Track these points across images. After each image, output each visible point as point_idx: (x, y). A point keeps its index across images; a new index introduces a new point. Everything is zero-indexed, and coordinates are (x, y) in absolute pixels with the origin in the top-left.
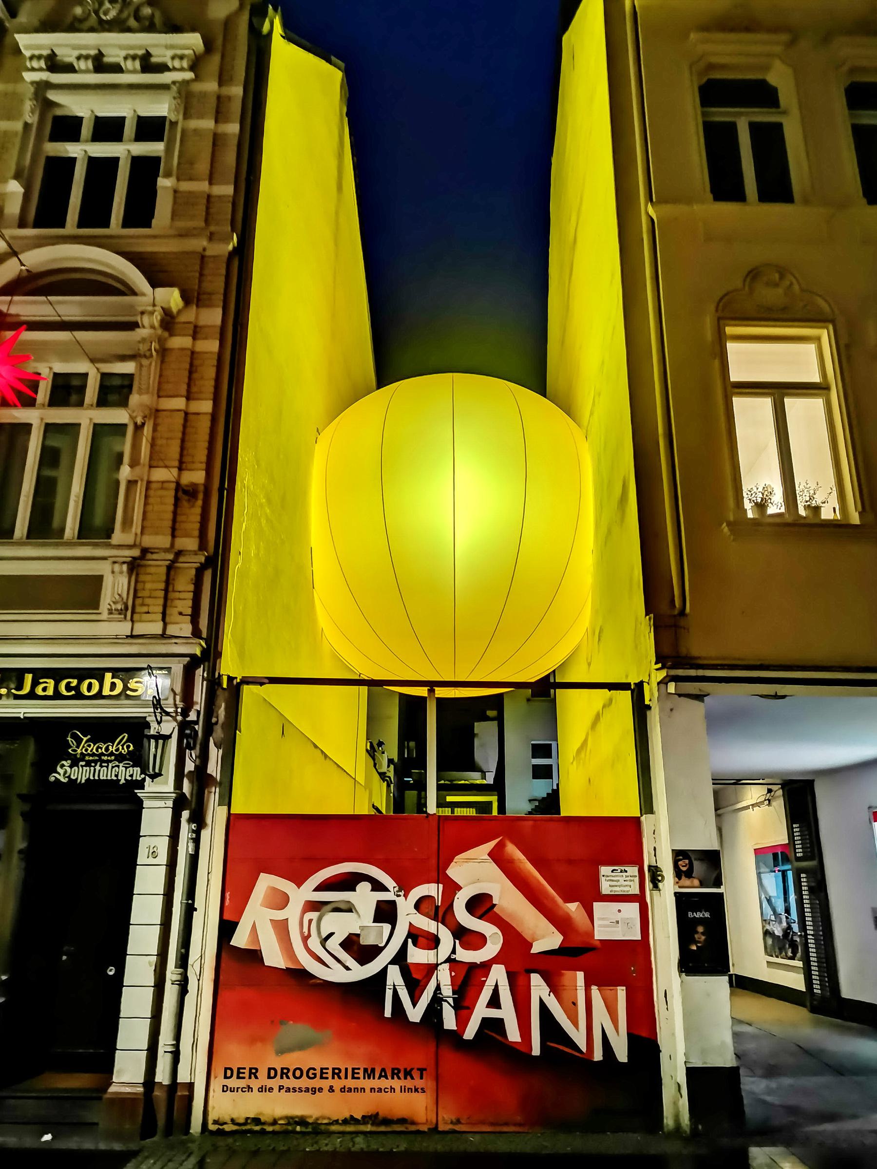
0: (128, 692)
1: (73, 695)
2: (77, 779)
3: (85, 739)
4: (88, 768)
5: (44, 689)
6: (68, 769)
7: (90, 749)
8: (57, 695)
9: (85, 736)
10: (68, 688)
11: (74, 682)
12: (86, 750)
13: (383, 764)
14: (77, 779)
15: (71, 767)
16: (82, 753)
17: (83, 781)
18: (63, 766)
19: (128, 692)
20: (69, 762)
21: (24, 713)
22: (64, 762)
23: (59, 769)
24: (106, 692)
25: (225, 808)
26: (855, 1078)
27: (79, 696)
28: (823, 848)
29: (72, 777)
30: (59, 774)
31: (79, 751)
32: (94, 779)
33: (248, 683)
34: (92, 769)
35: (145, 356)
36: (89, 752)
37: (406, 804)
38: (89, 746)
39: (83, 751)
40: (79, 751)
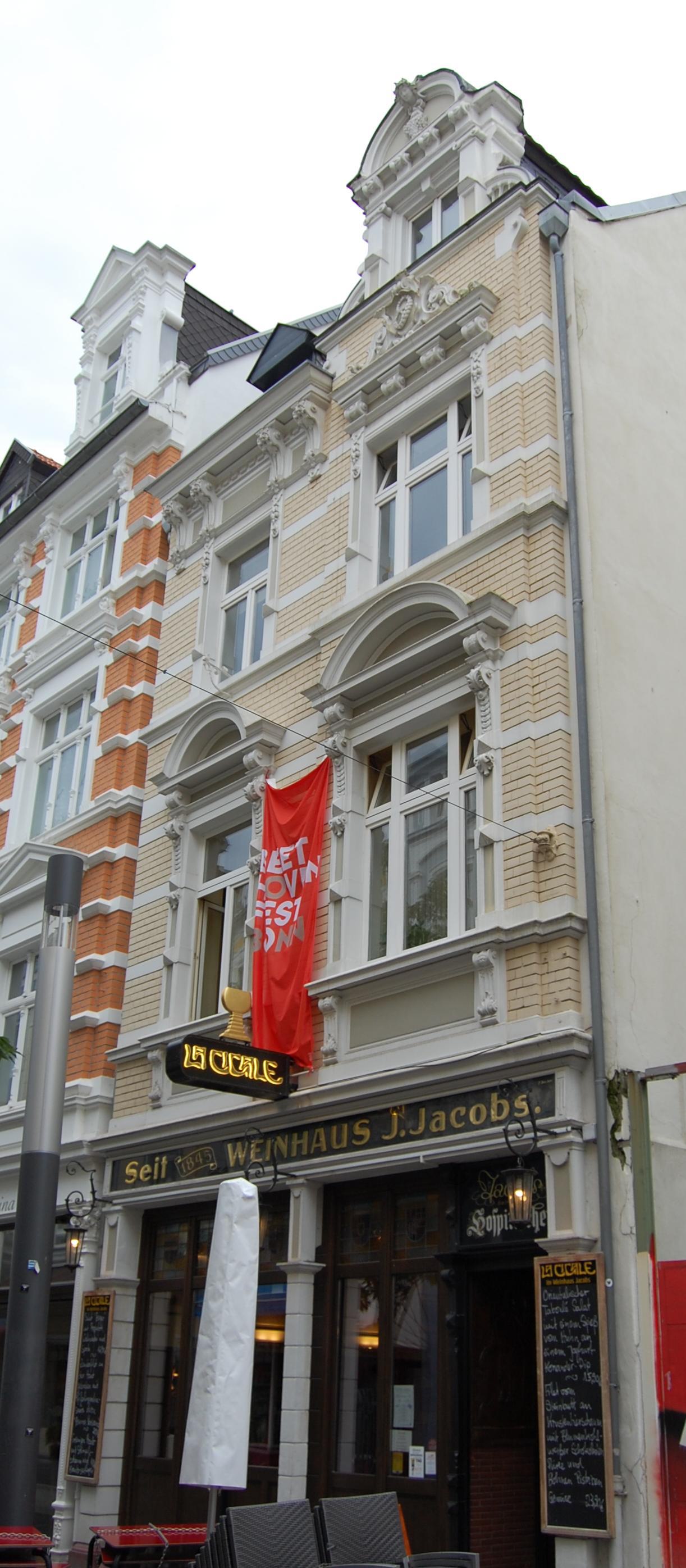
0: (516, 1114)
1: (633, 1152)
2: (492, 1231)
3: (494, 1180)
4: (501, 1216)
5: (438, 1124)
6: (483, 1219)
7: (500, 1192)
8: (451, 1130)
9: (494, 1176)
10: (459, 1119)
11: (463, 1110)
12: (497, 1194)
13: (628, 1128)
14: (492, 1231)
15: (485, 1216)
16: (493, 1198)
17: (499, 1233)
18: (477, 1216)
19: (516, 1114)
20: (483, 1209)
21: (424, 1157)
22: (478, 1212)
23: (475, 1221)
24: (494, 1117)
25: (647, 1255)
26: (105, 547)
27: (469, 1127)
28: (656, 1202)
29: (489, 1230)
30: (475, 1226)
31: (490, 1196)
32: (509, 1230)
33: (652, 1078)
34: (506, 1216)
35: (481, 690)
36: (500, 1195)
37: (140, 1236)
38: (499, 1188)
39: (495, 1195)
40: (490, 1196)
